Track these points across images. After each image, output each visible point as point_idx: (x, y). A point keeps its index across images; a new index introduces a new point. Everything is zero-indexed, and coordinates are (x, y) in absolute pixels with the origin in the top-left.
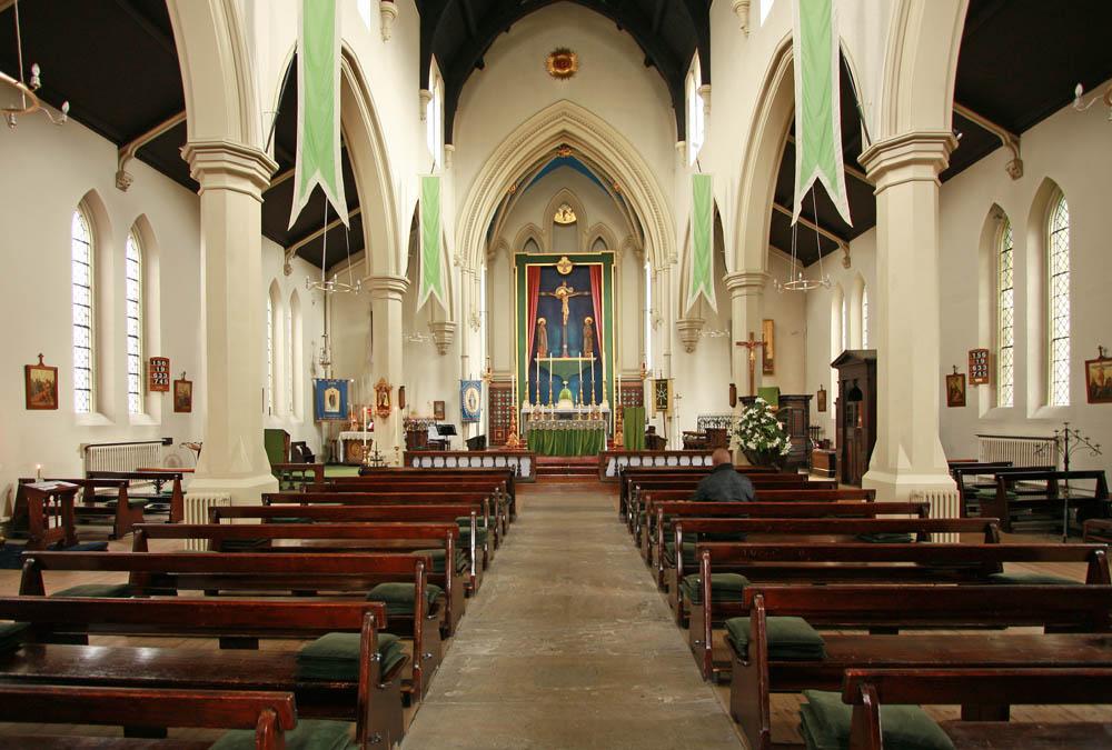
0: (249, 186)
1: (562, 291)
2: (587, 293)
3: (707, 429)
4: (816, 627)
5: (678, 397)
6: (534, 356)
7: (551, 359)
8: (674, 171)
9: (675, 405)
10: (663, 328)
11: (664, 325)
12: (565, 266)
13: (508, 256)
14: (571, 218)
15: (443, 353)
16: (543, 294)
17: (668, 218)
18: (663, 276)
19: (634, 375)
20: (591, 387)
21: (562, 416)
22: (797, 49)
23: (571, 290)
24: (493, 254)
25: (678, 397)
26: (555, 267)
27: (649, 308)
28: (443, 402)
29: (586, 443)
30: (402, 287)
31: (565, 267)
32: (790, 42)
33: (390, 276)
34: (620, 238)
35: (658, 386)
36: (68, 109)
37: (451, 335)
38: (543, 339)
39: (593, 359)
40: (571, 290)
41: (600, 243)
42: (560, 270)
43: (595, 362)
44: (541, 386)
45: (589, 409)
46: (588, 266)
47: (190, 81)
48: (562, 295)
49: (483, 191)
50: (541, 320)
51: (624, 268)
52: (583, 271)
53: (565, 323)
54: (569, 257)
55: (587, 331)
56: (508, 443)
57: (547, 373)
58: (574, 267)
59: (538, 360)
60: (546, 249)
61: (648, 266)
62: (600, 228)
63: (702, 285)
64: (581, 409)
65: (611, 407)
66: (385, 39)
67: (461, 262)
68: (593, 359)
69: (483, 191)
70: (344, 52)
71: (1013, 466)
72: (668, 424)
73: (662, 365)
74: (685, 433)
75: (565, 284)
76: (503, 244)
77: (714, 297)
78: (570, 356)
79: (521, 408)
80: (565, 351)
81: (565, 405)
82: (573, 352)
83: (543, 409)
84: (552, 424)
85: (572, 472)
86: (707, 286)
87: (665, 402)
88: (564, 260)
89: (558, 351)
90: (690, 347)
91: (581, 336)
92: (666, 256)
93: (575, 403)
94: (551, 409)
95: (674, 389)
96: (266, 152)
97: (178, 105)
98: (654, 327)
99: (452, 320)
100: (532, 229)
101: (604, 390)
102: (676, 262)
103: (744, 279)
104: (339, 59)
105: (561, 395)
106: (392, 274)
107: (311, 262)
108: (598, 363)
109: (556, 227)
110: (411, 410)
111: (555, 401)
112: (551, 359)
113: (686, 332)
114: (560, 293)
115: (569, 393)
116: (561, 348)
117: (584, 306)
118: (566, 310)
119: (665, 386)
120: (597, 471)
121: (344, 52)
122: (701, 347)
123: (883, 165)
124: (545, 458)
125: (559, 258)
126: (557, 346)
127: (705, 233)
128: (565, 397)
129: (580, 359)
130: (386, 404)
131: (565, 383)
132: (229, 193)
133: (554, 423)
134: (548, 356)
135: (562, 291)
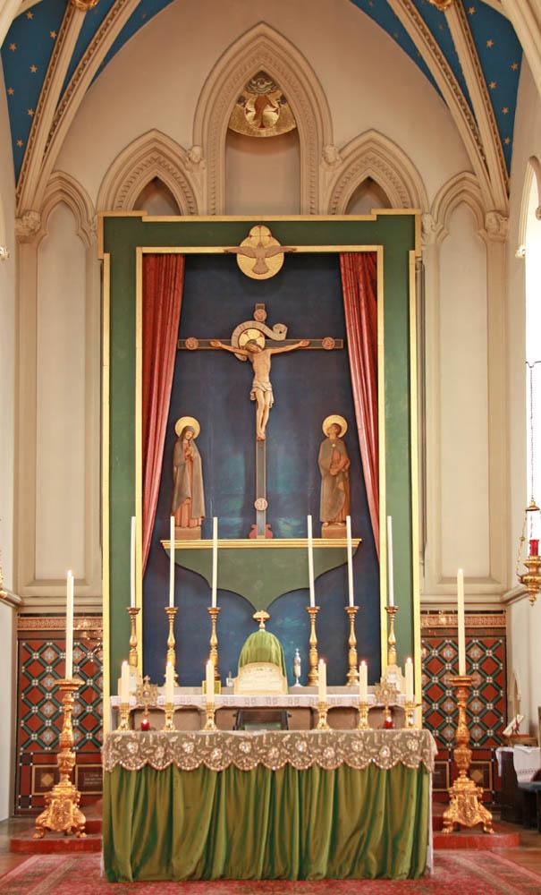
2: (328, 343)
5: (271, 670)
6: (158, 535)
7: (215, 543)
12: (259, 254)
13: (83, 234)
16: (192, 343)
19: (486, 594)
20: (343, 620)
21: (247, 716)
23: (279, 332)
26: (231, 259)
29: (347, 826)
31: (260, 259)
36: (216, 641)
38: (191, 479)
40: (279, 332)
42: (246, 264)
43: (357, 552)
44: (181, 619)
45: (359, 692)
46: (335, 257)
48: (250, 349)
53: (261, 432)
54: (276, 229)
55: (332, 458)
58: (289, 257)
59: (171, 545)
64: (322, 694)
68: (350, 543)
71: (239, 669)
75: (261, 314)
78: (274, 532)
79: (114, 692)
81: (260, 684)
82: (284, 524)
83: (171, 694)
84: (206, 747)
88: (260, 235)
89: (237, 521)
91: (311, 471)
100: (158, 151)
105: (246, 649)
111: (227, 671)
112: (215, 543)
114: (244, 340)
115: (273, 644)
116: (250, 511)
117: (325, 384)
125: (243, 230)
126: (238, 504)
128: (261, 657)
129: (311, 542)
131: (261, 615)
133: (220, 742)
134: (206, 534)
135: (253, 334)
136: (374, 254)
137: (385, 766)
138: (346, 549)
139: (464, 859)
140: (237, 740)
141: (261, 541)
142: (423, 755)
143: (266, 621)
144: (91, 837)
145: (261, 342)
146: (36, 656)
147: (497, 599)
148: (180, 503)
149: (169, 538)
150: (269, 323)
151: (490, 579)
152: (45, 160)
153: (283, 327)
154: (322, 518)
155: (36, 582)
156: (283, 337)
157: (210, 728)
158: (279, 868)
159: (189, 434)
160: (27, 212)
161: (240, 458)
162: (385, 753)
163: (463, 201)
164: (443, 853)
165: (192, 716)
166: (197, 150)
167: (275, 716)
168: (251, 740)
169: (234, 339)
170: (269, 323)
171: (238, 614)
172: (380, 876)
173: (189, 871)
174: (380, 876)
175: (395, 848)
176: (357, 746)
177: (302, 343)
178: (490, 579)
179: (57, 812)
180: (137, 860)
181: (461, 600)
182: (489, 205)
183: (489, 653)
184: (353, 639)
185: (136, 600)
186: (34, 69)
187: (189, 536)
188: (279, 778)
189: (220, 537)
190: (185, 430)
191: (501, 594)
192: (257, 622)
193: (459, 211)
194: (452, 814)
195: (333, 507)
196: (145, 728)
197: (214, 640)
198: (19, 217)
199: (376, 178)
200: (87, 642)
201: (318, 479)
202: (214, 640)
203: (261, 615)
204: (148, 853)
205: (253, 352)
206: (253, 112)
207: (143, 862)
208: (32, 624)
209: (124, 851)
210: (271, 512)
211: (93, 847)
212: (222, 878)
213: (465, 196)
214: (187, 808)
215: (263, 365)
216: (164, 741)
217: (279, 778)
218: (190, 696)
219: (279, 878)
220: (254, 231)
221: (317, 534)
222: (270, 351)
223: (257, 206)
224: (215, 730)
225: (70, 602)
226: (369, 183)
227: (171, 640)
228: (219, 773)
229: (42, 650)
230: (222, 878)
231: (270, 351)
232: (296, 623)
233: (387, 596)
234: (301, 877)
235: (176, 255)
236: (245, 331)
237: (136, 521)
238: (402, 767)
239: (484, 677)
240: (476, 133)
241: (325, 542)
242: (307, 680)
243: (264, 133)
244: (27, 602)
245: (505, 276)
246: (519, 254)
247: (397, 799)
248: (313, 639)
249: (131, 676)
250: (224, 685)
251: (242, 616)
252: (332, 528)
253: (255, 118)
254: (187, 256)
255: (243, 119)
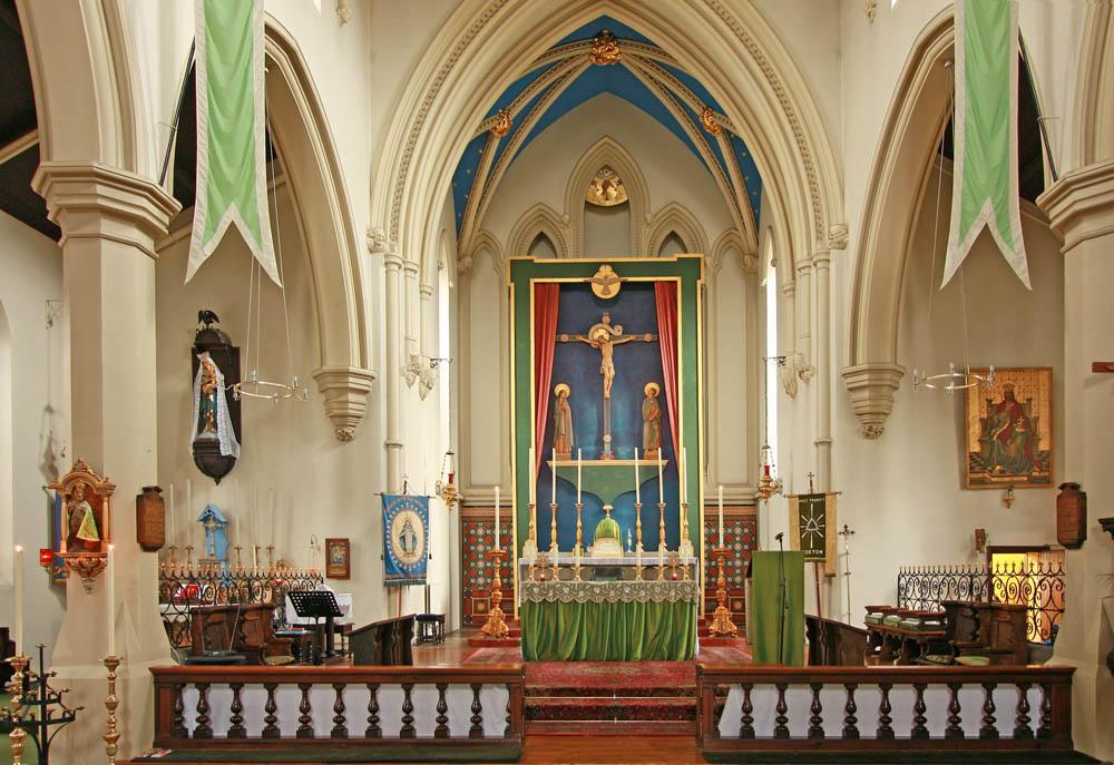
0: (135, 234)
1: (602, 332)
2: (648, 337)
3: (945, 604)
4: (175, 196)
5: (846, 532)
7: (580, 463)
8: (839, 53)
9: (841, 550)
10: (811, 394)
11: (817, 382)
12: (606, 282)
13: (497, 268)
14: (615, 195)
15: (345, 438)
16: (565, 338)
17: (826, 154)
18: (810, 282)
19: (741, 494)
20: (656, 515)
21: (601, 571)
22: (958, 34)
24: (468, 260)
25: (846, 532)
26: (588, 285)
27: (772, 350)
28: (346, 541)
29: (652, 632)
30: (159, 219)
31: (606, 286)
32: (950, 22)
33: (101, 165)
34: (713, 234)
35: (803, 509)
37: (362, 398)
38: (565, 424)
39: (661, 463)
41: (673, 243)
42: (597, 289)
45: (661, 556)
46: (653, 283)
47: (39, 65)
49: (431, 97)
50: (561, 387)
51: (721, 285)
52: (641, 296)
53: (607, 394)
54: (615, 267)
55: (649, 409)
56: (486, 628)
57: (572, 489)
58: (624, 285)
59: (553, 464)
60: (570, 250)
61: (770, 280)
62: (673, 213)
63: (987, 208)
64: (640, 557)
65: (697, 554)
66: (343, 21)
67: (386, 246)
68: (661, 463)
69: (431, 97)
70: (269, 30)
72: (824, 588)
73: (811, 460)
74: (871, 609)
75: (606, 319)
76: (487, 243)
77: (1020, 244)
78: (615, 456)
79: (520, 555)
80: (607, 448)
81: (607, 551)
82: (622, 451)
83: (555, 556)
84: (579, 589)
85: (624, 712)
86: (1002, 216)
87: (820, 543)
88: (605, 271)
89: (592, 448)
90: (873, 432)
91: (636, 417)
92: (819, 232)
93: (625, 548)
94: (576, 558)
95: (839, 514)
96: (161, 184)
97: (26, 119)
98: (789, 389)
99: (363, 365)
100: (542, 215)
101: (683, 522)
102: (843, 246)
103: (866, 376)
104: (262, 44)
105: (599, 530)
106: (111, 163)
107: (22, 220)
108: (672, 469)
109: (591, 216)
110: (277, 557)
111: (587, 543)
113: (866, 394)
114: (596, 336)
115: (614, 526)
116: (600, 443)
117: (646, 364)
118: (609, 368)
119: (821, 508)
120: (690, 712)
121: (269, 30)
122: (896, 424)
123: (1077, 207)
124: (558, 669)
125: (595, 267)
126: (592, 438)
127: (998, 65)
128: (607, 535)
129: (637, 462)
130: (87, 532)
131: (608, 507)
132: (103, 241)
133: (583, 587)
134: (574, 457)
135: (602, 332)
136: (675, 282)
137: (672, 601)
138: (658, 466)
139: (718, 651)
140: (593, 586)
141: (607, 462)
142: (693, 594)
143: (611, 511)
144: (512, 639)
145: (607, 337)
146: (473, 532)
147: (751, 497)
148: (558, 438)
149: (551, 459)
150: (612, 325)
151: (747, 485)
152: (475, 223)
153: (620, 327)
154: (645, 447)
155: (471, 486)
156: (620, 333)
157: (578, 580)
158: (615, 655)
159: (563, 395)
160: (465, 256)
161: (594, 410)
162: (673, 593)
163: (732, 247)
164: (707, 649)
165: (1075, 535)
166: (567, 216)
167: (612, 571)
168: (600, 587)
169: (590, 335)
170: (612, 325)
171: (594, 507)
172: (669, 659)
173: (567, 656)
174: (669, 659)
175: (677, 644)
176: (658, 590)
177: (632, 338)
178: (747, 485)
179: (493, 625)
180: (540, 650)
181: (721, 498)
182: (747, 251)
183: (746, 531)
184: (662, 523)
185: (533, 499)
186: (469, 171)
187: (565, 459)
188: (615, 607)
189: (582, 459)
190: (561, 392)
191: (753, 494)
192: (605, 512)
193: (727, 254)
194: (714, 627)
195: (651, 440)
196: (542, 580)
197: (579, 524)
198: (459, 260)
199: (677, 231)
200: (506, 521)
201: (642, 421)
202: (579, 524)
203: (608, 507)
204: (545, 646)
205: (601, 344)
206: (601, 191)
207: (543, 651)
208: (470, 512)
209: (534, 642)
210: (614, 443)
211: (515, 644)
212: (585, 660)
213: (732, 244)
214: (565, 623)
215: (608, 351)
216: (553, 587)
217: (615, 607)
218: (567, 558)
219: (615, 660)
220: (602, 268)
221: (641, 457)
222: (612, 343)
223: (606, 252)
224: (580, 580)
225: (497, 498)
226: (673, 236)
227: (554, 524)
228: (583, 604)
229: (476, 528)
230: (585, 660)
231: (612, 343)
232: (629, 512)
233: (683, 497)
234: (627, 660)
235: (555, 283)
236: (597, 330)
237: (532, 451)
238: (681, 601)
239: (479, 560)
240: (735, 199)
241: (645, 462)
242: (634, 549)
243: (608, 203)
244: (467, 499)
245: (756, 296)
246: (763, 284)
247: (679, 617)
248: (639, 523)
249: (531, 550)
250: (586, 551)
251: (597, 508)
252: (651, 453)
253: (603, 194)
254: (561, 284)
255: (595, 195)
